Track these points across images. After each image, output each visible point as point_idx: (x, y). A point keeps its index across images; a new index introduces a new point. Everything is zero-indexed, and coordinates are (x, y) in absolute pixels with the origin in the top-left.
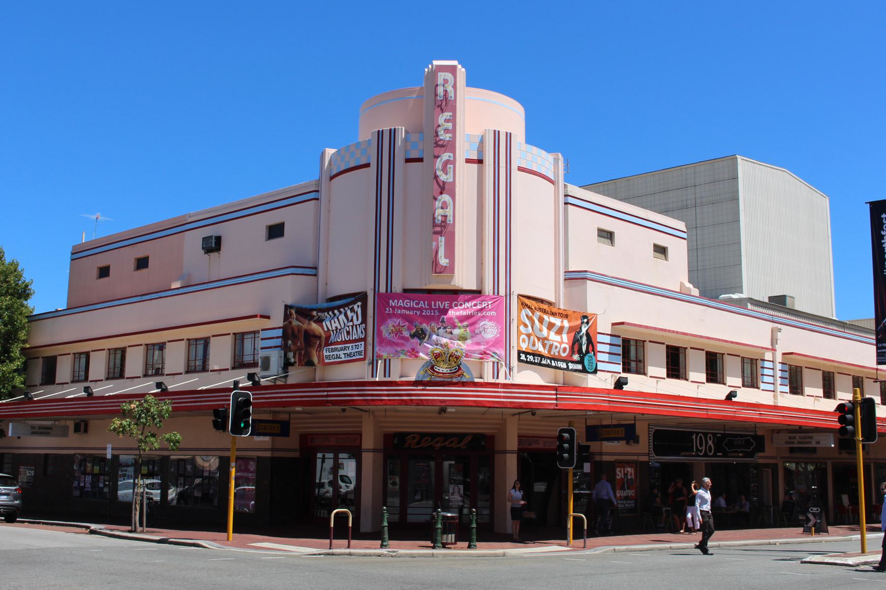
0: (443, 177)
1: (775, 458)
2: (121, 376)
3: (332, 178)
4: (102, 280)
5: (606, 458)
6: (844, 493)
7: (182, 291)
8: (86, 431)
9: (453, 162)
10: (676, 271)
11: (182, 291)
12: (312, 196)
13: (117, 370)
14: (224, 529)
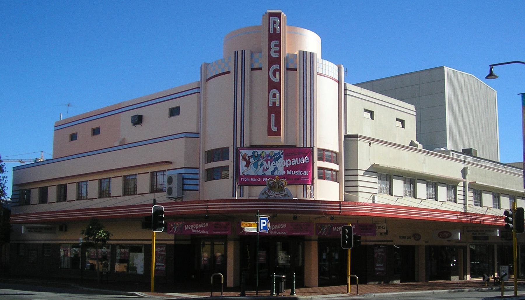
0: (274, 79)
1: (465, 242)
2: (65, 199)
3: (208, 80)
4: (172, 118)
5: (368, 243)
6: (140, 275)
7: (119, 148)
8: (66, 230)
9: (279, 70)
10: (410, 132)
11: (119, 148)
12: (196, 90)
13: (62, 197)
14: (345, 283)
